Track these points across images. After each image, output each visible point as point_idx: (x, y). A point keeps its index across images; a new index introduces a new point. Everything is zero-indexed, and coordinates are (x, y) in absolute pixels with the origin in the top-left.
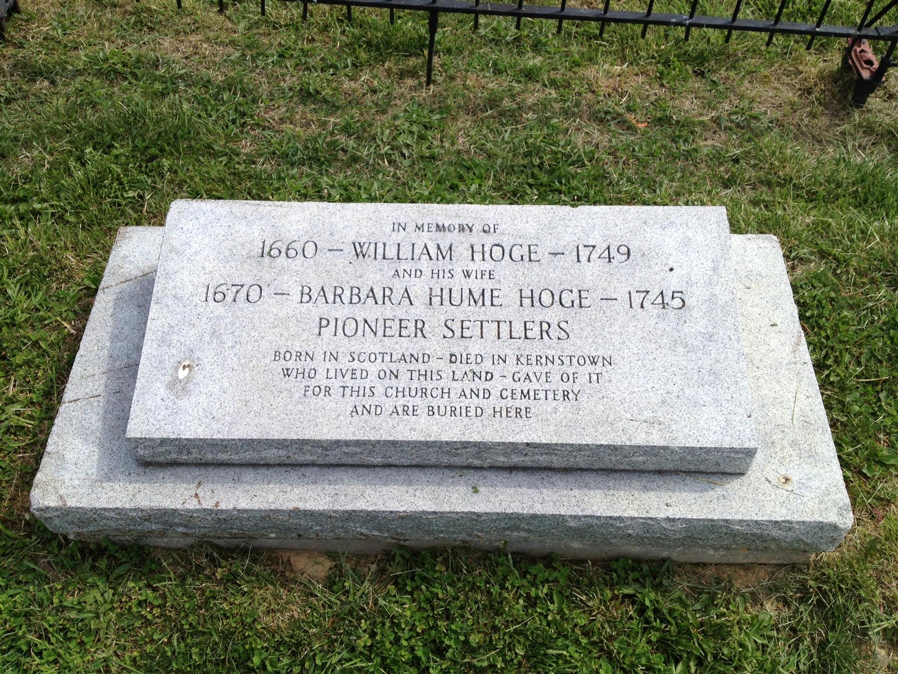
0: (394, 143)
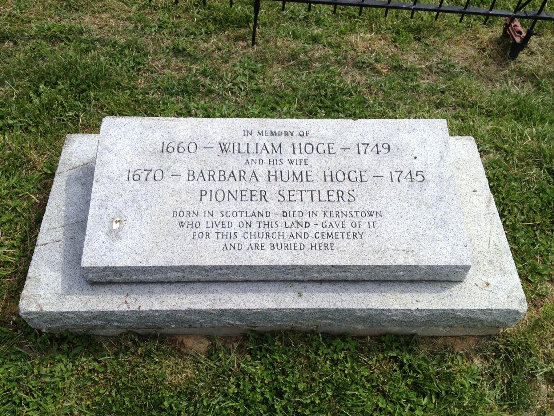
0: (234, 81)
